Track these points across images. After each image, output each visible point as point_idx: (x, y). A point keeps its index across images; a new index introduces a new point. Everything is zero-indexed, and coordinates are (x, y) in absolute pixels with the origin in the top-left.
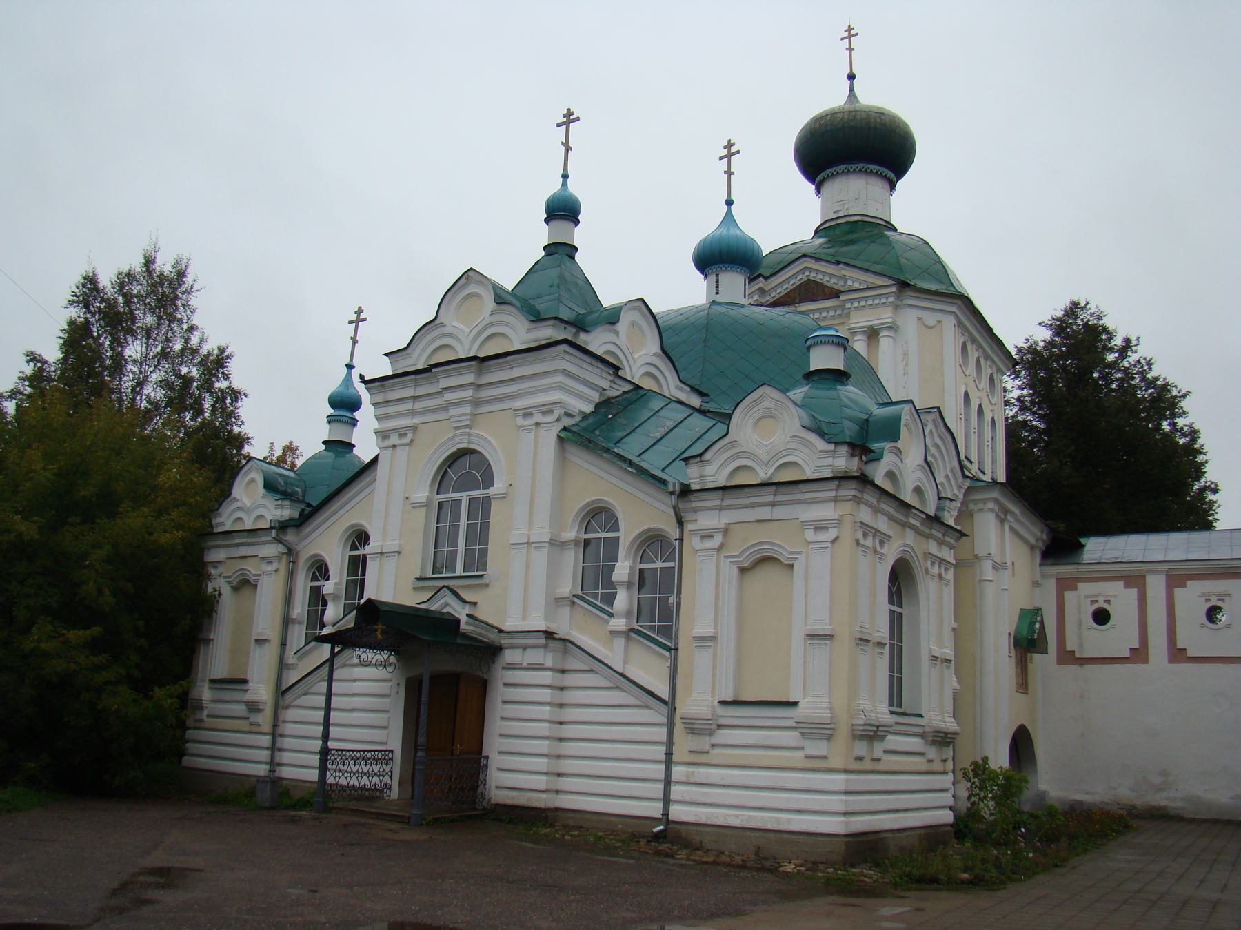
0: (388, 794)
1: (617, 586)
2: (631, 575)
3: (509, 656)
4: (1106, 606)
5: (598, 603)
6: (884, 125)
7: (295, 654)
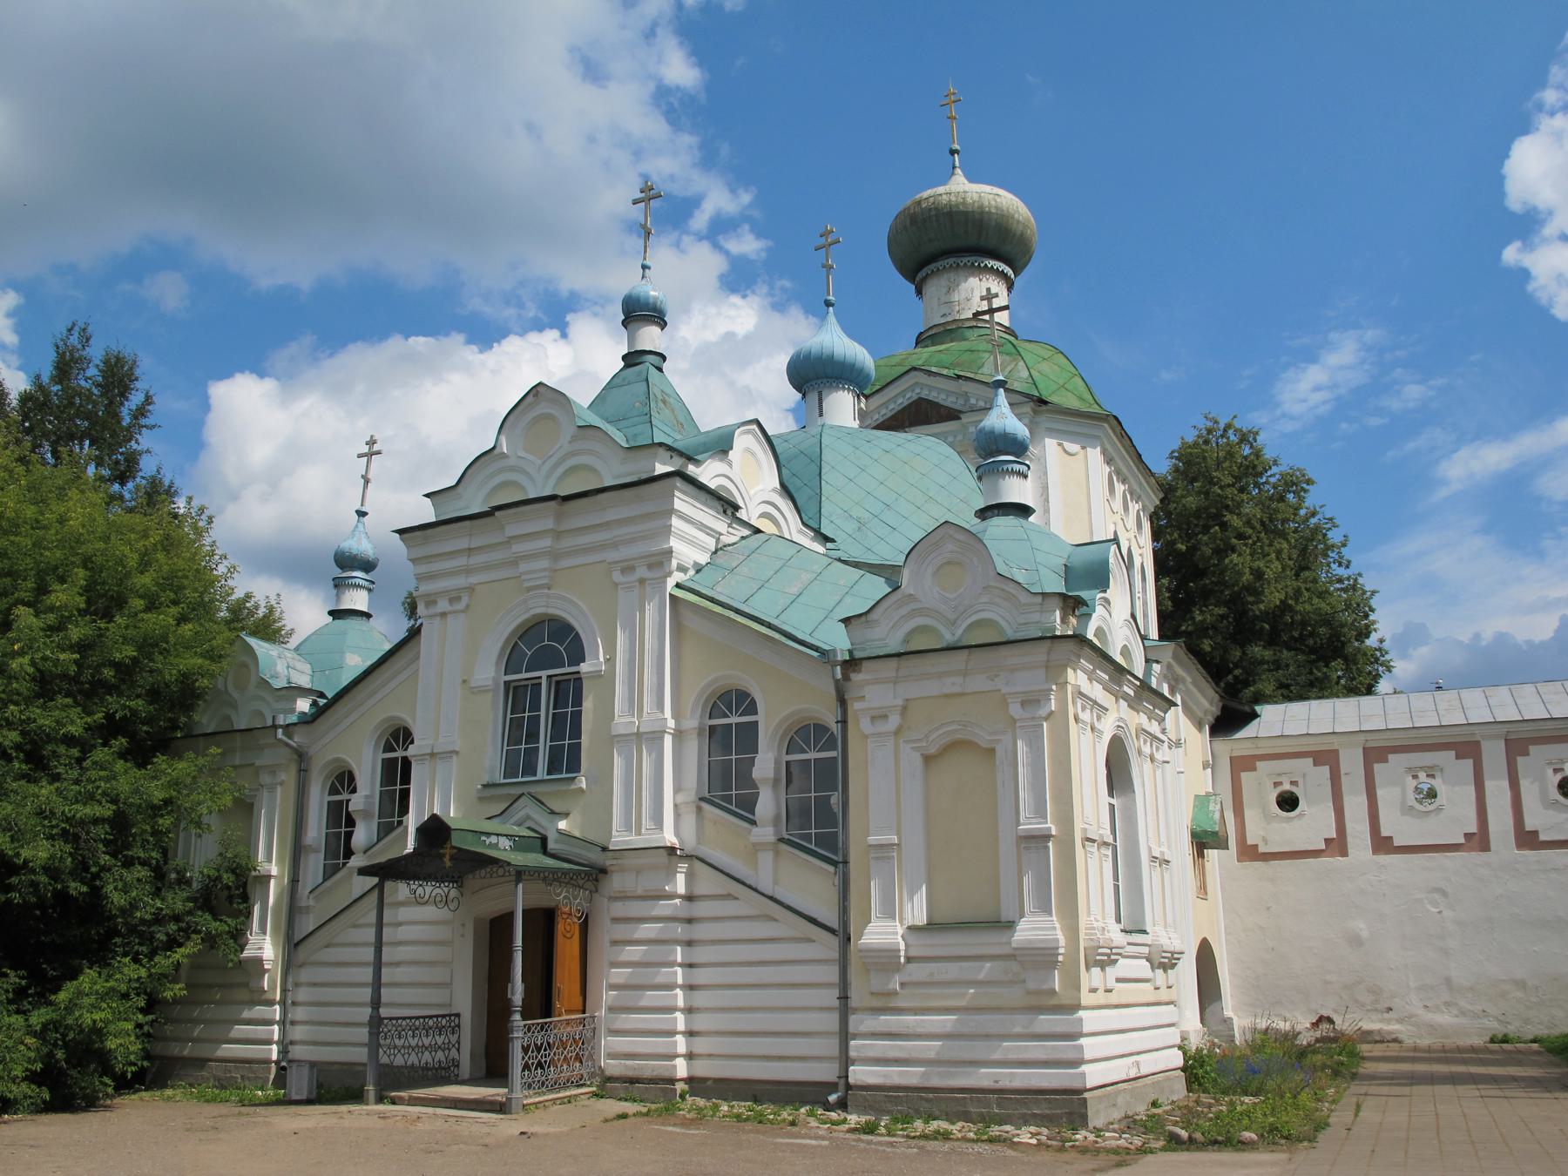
0: (456, 1072)
1: (759, 785)
2: (777, 770)
3: (616, 883)
5: (733, 808)
6: (982, 213)
7: (311, 892)
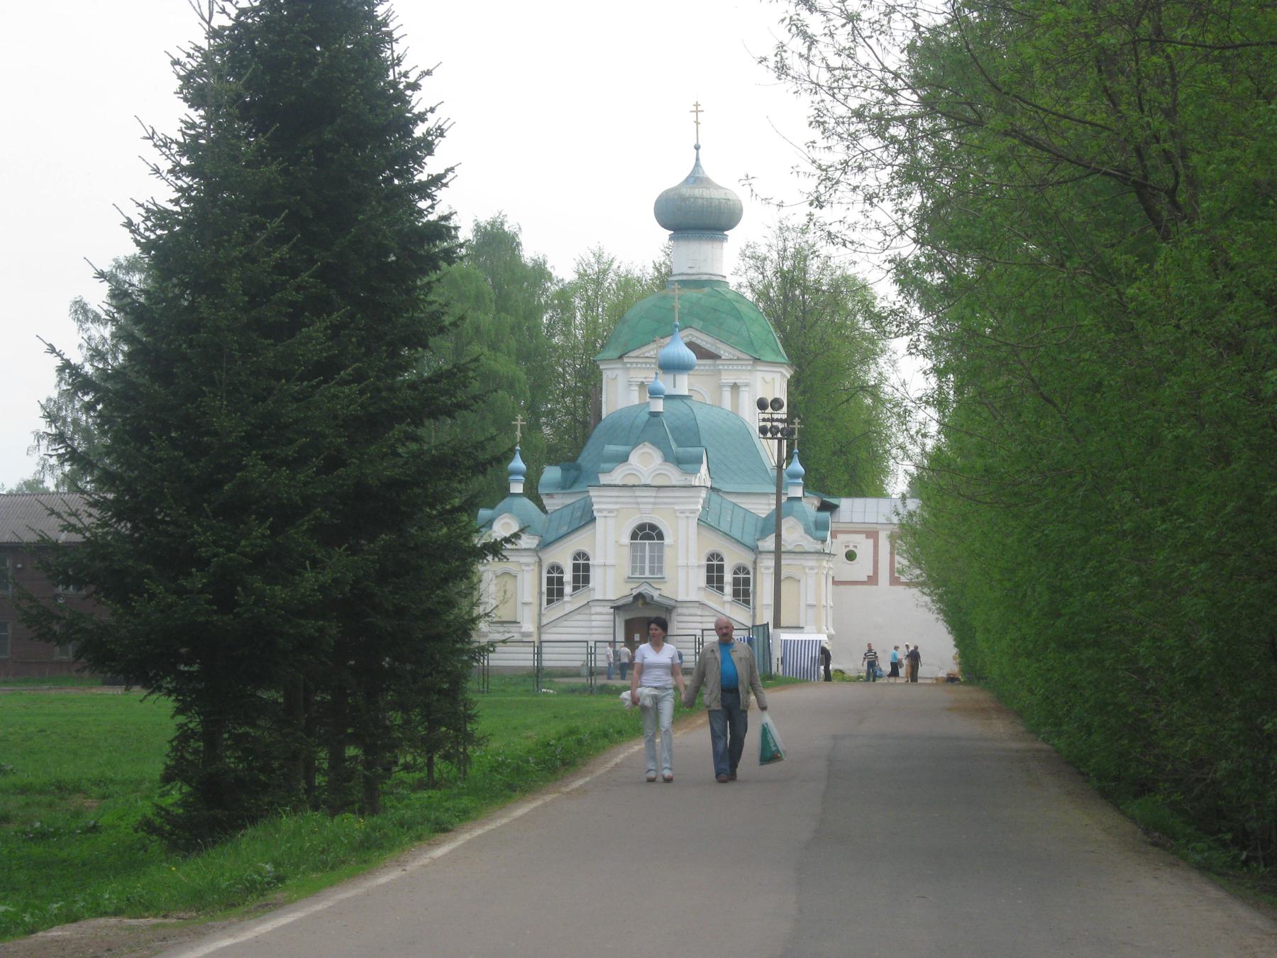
3: (680, 610)
4: (854, 549)
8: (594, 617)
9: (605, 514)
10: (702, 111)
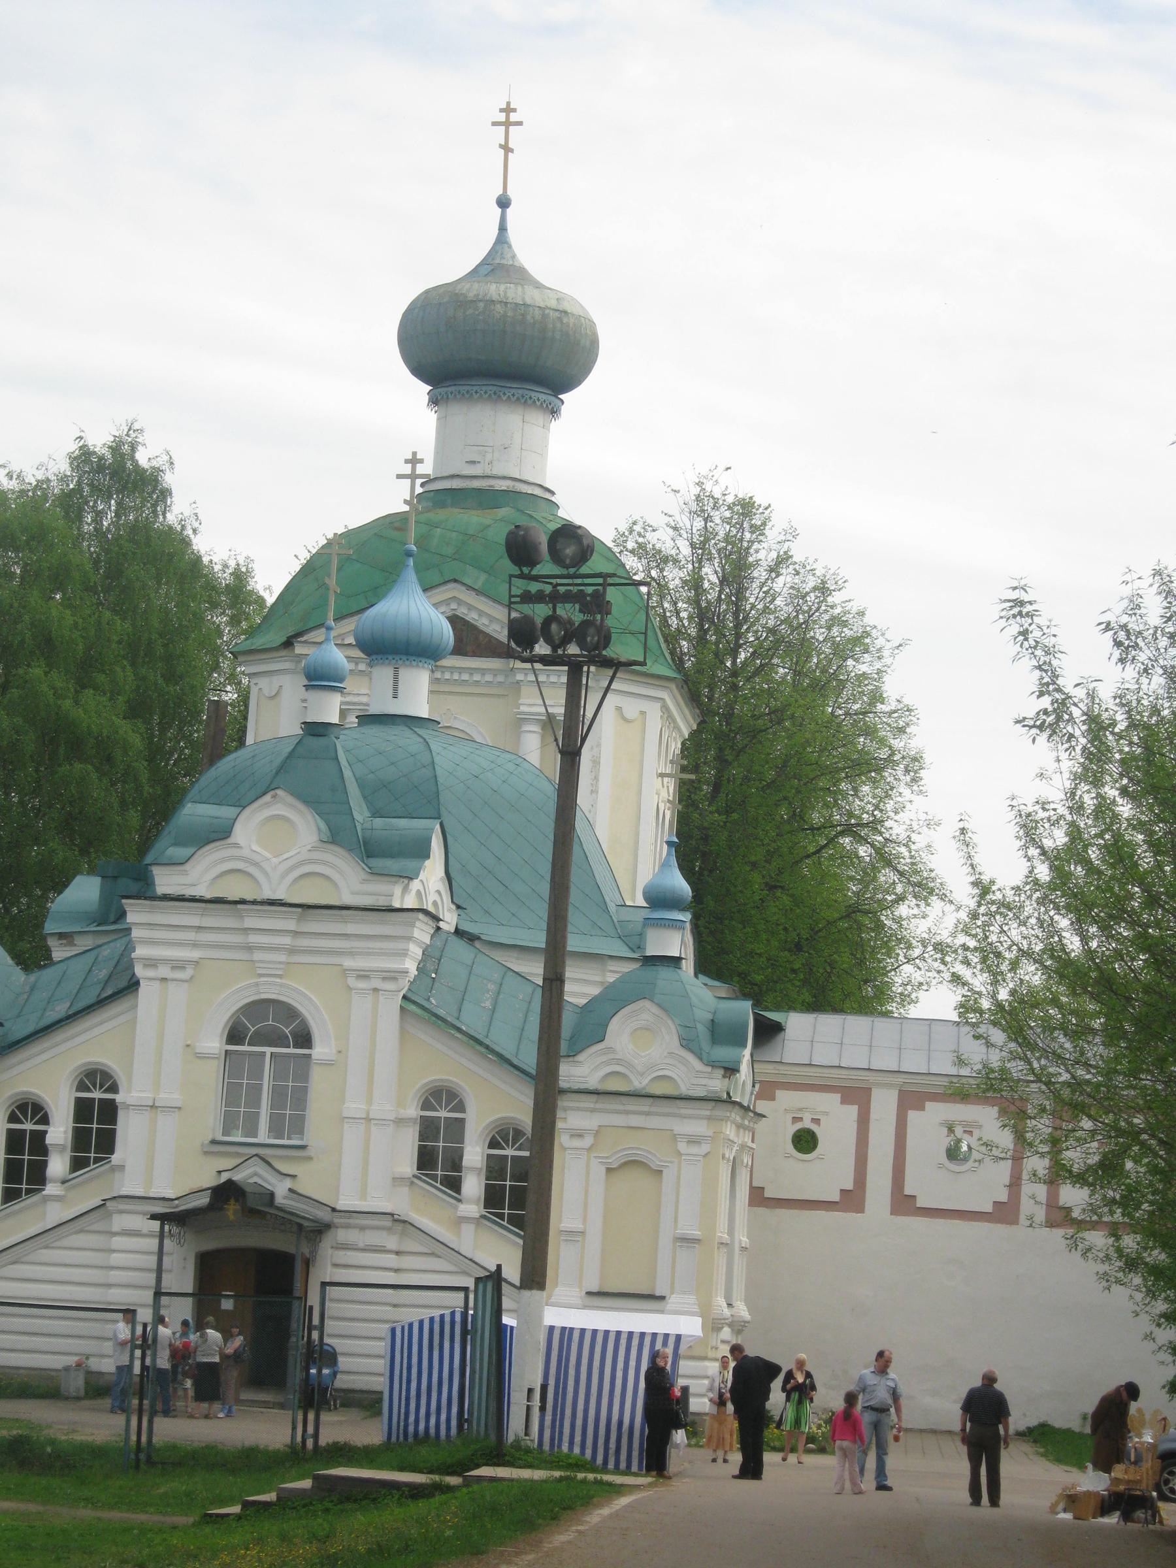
3: (342, 1235)
4: (814, 1127)
8: (118, 1242)
9: (163, 971)
10: (520, 123)
